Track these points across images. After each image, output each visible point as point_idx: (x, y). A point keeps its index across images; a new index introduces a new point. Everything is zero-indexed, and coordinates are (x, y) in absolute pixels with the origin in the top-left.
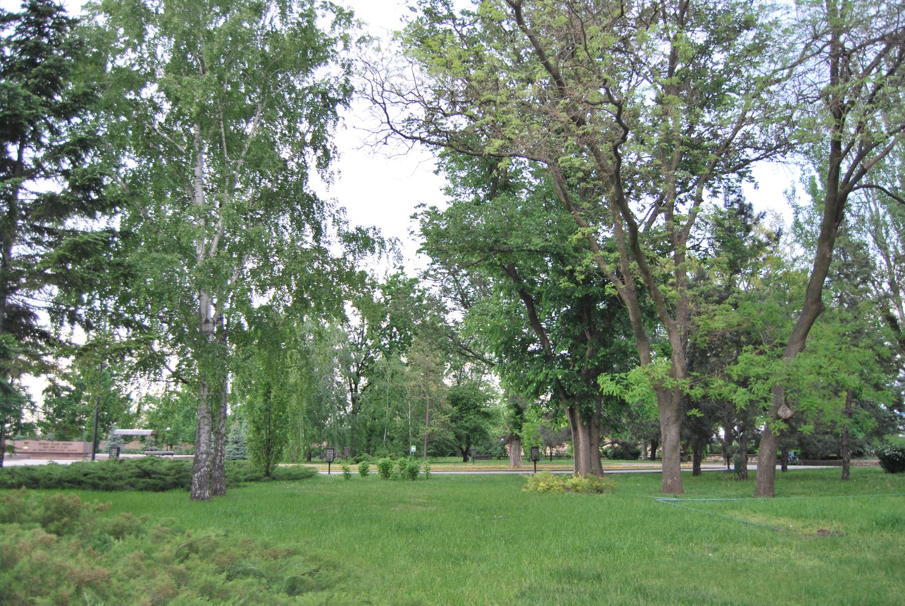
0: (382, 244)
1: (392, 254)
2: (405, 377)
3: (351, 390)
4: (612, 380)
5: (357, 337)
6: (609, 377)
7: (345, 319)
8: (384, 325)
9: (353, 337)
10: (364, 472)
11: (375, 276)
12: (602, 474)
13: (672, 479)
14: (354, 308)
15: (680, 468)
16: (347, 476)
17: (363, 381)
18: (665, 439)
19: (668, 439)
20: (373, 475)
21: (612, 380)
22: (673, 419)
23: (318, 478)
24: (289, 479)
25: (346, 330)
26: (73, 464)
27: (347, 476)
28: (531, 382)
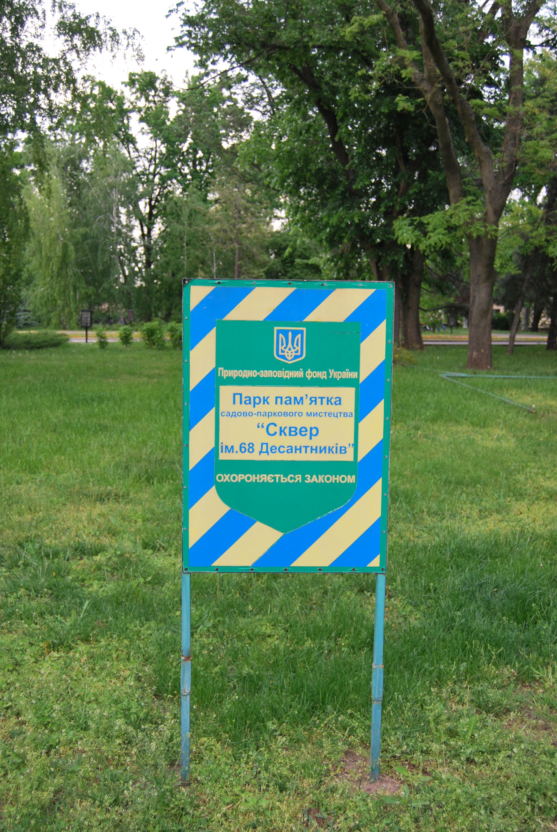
0: (114, 36)
1: (130, 52)
2: (207, 218)
3: (143, 235)
4: (410, 225)
5: (147, 164)
6: (407, 221)
7: (129, 140)
8: (185, 147)
9: (142, 165)
10: (126, 339)
11: (169, 79)
12: (422, 347)
13: (478, 351)
14: (144, 125)
15: (490, 339)
16: (103, 344)
17: (158, 228)
18: (474, 301)
19: (477, 301)
20: (137, 343)
21: (410, 225)
22: (484, 276)
23: (68, 346)
24: (26, 348)
25: (134, 155)
26: (39, 334)
27: (103, 344)
28: (326, 225)
